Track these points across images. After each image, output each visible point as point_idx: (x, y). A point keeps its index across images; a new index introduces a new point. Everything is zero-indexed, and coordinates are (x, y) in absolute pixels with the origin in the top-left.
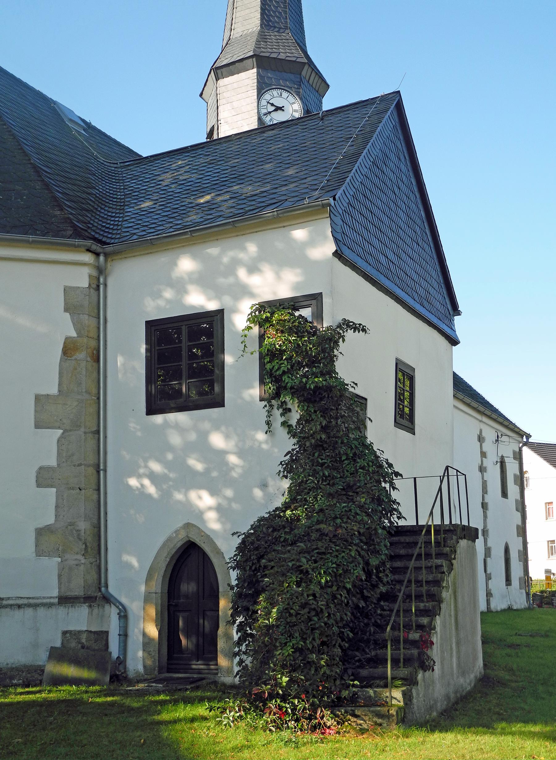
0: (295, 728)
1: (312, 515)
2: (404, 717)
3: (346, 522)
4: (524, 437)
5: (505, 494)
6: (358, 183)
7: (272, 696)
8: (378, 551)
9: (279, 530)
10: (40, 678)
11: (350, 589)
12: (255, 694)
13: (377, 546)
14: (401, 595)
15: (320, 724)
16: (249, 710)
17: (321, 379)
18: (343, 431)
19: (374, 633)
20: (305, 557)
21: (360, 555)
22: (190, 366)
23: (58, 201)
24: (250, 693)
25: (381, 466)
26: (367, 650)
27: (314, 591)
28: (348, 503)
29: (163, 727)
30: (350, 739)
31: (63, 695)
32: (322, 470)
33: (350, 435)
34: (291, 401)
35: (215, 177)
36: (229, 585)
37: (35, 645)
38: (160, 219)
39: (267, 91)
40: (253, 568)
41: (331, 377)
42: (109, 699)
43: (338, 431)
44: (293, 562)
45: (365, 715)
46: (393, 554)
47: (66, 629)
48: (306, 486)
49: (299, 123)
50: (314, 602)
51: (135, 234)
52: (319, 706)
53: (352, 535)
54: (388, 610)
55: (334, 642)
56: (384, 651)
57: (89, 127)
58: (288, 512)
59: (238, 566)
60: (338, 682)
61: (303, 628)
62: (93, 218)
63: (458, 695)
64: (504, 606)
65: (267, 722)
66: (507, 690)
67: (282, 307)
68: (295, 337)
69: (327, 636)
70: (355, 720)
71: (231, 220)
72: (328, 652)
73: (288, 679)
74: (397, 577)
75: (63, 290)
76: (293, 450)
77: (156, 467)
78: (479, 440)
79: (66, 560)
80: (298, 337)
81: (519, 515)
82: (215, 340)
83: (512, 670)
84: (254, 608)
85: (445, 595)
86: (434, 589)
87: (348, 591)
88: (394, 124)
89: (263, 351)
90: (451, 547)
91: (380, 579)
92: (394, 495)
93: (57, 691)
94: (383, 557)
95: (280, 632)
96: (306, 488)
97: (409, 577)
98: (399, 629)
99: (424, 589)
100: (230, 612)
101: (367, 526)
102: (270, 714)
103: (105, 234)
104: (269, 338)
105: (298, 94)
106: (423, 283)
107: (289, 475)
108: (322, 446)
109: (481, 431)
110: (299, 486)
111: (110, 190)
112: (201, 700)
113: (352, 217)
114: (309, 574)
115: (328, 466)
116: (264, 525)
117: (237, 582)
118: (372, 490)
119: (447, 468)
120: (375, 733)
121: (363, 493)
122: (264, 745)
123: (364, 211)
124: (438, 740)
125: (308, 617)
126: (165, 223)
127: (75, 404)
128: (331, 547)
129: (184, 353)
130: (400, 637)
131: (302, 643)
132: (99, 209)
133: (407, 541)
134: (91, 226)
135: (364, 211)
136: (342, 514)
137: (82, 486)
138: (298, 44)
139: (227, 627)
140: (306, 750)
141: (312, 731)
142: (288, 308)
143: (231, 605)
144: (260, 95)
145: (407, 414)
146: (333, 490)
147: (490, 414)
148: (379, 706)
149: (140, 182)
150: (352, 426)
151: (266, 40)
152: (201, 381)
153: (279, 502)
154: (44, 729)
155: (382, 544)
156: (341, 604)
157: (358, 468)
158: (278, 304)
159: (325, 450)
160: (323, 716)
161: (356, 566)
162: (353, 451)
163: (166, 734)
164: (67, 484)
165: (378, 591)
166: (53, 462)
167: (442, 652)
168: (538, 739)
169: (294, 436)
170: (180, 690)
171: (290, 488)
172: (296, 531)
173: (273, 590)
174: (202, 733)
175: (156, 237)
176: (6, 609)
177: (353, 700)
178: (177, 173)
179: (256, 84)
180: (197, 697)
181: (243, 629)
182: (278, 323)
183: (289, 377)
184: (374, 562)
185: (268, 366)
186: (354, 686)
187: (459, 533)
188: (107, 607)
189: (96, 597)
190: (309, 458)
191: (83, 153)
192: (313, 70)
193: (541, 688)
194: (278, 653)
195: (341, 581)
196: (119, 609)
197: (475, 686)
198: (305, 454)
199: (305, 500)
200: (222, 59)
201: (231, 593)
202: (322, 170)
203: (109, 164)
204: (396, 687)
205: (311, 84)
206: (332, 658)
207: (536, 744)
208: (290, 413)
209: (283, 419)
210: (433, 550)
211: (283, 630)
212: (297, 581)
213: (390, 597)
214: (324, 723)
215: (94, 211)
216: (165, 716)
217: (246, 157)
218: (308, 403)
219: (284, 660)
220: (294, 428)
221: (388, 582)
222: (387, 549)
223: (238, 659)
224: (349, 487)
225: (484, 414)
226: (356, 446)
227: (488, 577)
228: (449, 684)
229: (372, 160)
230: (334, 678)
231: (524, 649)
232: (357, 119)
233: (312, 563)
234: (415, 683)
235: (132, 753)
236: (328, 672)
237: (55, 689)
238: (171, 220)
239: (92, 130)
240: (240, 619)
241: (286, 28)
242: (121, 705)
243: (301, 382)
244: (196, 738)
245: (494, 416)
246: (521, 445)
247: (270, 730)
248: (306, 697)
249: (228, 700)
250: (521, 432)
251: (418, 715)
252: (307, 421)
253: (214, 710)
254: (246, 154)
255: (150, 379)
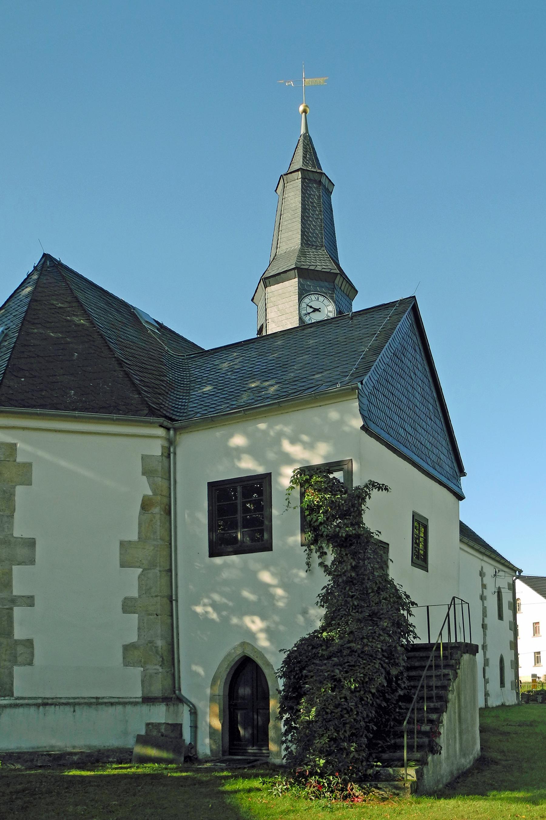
0: (331, 797)
1: (344, 636)
2: (417, 789)
3: (372, 642)
4: (517, 572)
5: (501, 617)
6: (381, 371)
7: (312, 774)
8: (397, 664)
9: (317, 648)
10: (130, 757)
11: (374, 693)
12: (299, 773)
13: (396, 660)
14: (415, 697)
15: (350, 794)
16: (294, 784)
17: (351, 529)
18: (369, 570)
19: (393, 726)
20: (338, 669)
21: (382, 667)
22: (244, 519)
23: (136, 386)
24: (294, 771)
25: (400, 597)
26: (388, 740)
27: (345, 695)
28: (374, 626)
29: (226, 796)
30: (374, 806)
31: (148, 771)
32: (352, 601)
33: (375, 573)
34: (327, 546)
35: (263, 366)
36: (277, 690)
37: (125, 733)
38: (219, 400)
39: (306, 296)
40: (297, 677)
41: (360, 527)
42: (184, 774)
43: (365, 570)
44: (329, 673)
45: (386, 788)
46: (409, 666)
47: (149, 722)
48: (339, 613)
49: (333, 322)
50: (346, 703)
51: (198, 412)
52: (349, 781)
53: (376, 652)
54: (405, 709)
55: (361, 734)
56: (402, 740)
57: (161, 327)
58: (325, 634)
59: (284, 675)
60: (364, 764)
61: (337, 723)
62: (165, 400)
63: (460, 772)
64: (499, 703)
65: (308, 793)
66: (498, 766)
67: (319, 471)
68: (329, 495)
69: (356, 729)
70: (378, 791)
71: (276, 401)
72: (356, 741)
73: (324, 761)
74: (412, 683)
75: (141, 458)
76: (328, 585)
77: (216, 597)
78: (481, 575)
79: (147, 669)
80: (332, 495)
81: (512, 633)
82: (264, 498)
83: (503, 752)
84: (297, 708)
85: (450, 696)
86: (442, 692)
87: (373, 695)
88: (411, 322)
89: (303, 507)
90: (456, 660)
91: (399, 685)
92: (411, 620)
93: (143, 767)
94: (401, 668)
95: (318, 726)
96: (339, 615)
97: (422, 684)
98: (414, 723)
99: (434, 692)
100: (279, 710)
101: (388, 645)
102: (310, 787)
103: (175, 413)
104: (308, 495)
105: (332, 299)
106: (435, 450)
107: (325, 605)
108: (352, 582)
109: (482, 568)
110: (334, 613)
111: (179, 377)
112: (256, 776)
113: (376, 398)
114: (342, 682)
115: (357, 598)
116: (305, 643)
117: (283, 688)
118: (393, 617)
119: (454, 598)
120: (393, 800)
121: (385, 619)
122: (306, 810)
123: (386, 392)
124: (443, 805)
125: (341, 714)
126: (223, 403)
127: (152, 548)
128: (359, 661)
129: (239, 508)
130: (414, 729)
131: (336, 734)
132: (170, 393)
133: (421, 655)
134: (163, 406)
135: (386, 392)
136: (369, 635)
137: (159, 612)
138: (332, 259)
139: (277, 721)
140: (339, 814)
141: (344, 800)
142: (324, 472)
143: (279, 705)
144: (300, 300)
145: (421, 555)
146: (361, 616)
147: (490, 554)
148: (397, 781)
149: (203, 371)
150: (377, 566)
151: (305, 256)
152: (252, 530)
153: (319, 624)
154: (134, 795)
155: (401, 658)
156: (367, 705)
157: (381, 599)
158: (316, 469)
159: (354, 585)
160: (353, 789)
161: (379, 675)
162: (377, 586)
163: (229, 801)
164: (147, 611)
165: (397, 694)
166: (135, 594)
167: (448, 740)
168: (521, 803)
169: (329, 574)
170: (239, 768)
171: (326, 615)
172: (331, 648)
173: (313, 694)
174: (257, 801)
175: (216, 415)
176: (102, 706)
177: (377, 777)
178: (233, 363)
179: (297, 291)
180: (253, 773)
181: (288, 723)
182: (315, 484)
183: (324, 527)
184: (394, 672)
185: (309, 518)
186: (377, 766)
187: (462, 649)
188: (180, 705)
189: (172, 698)
190: (341, 591)
191: (157, 347)
192: (344, 279)
193: (525, 765)
194: (316, 742)
195: (367, 688)
196: (190, 707)
197: (473, 765)
198: (338, 588)
199: (339, 624)
200: (270, 271)
201: (279, 696)
202: (351, 360)
203: (177, 357)
204: (411, 766)
205: (343, 290)
206: (360, 746)
207: (519, 807)
208: (326, 556)
209: (320, 560)
210: (442, 663)
211: (320, 724)
212: (331, 687)
213: (407, 699)
214: (354, 794)
215: (166, 394)
216: (228, 787)
217: (290, 350)
218: (341, 548)
219: (321, 747)
220: (330, 567)
221: (405, 687)
222: (405, 662)
223: (285, 745)
224: (373, 614)
225: (486, 554)
226: (379, 582)
227: (486, 682)
228: (453, 764)
229: (393, 351)
230: (361, 760)
231: (514, 735)
232: (381, 319)
233: (344, 673)
234: (426, 763)
235: (202, 815)
236: (357, 756)
237: (142, 766)
238: (228, 401)
239: (164, 330)
240: (286, 716)
241: (322, 246)
242: (193, 779)
243: (335, 531)
244: (252, 804)
245: (497, 558)
246: (514, 578)
247: (311, 799)
248: (339, 774)
249: (277, 776)
250: (514, 568)
251: (427, 787)
252: (340, 562)
253: (266, 784)
254: (289, 347)
255: (211, 528)
